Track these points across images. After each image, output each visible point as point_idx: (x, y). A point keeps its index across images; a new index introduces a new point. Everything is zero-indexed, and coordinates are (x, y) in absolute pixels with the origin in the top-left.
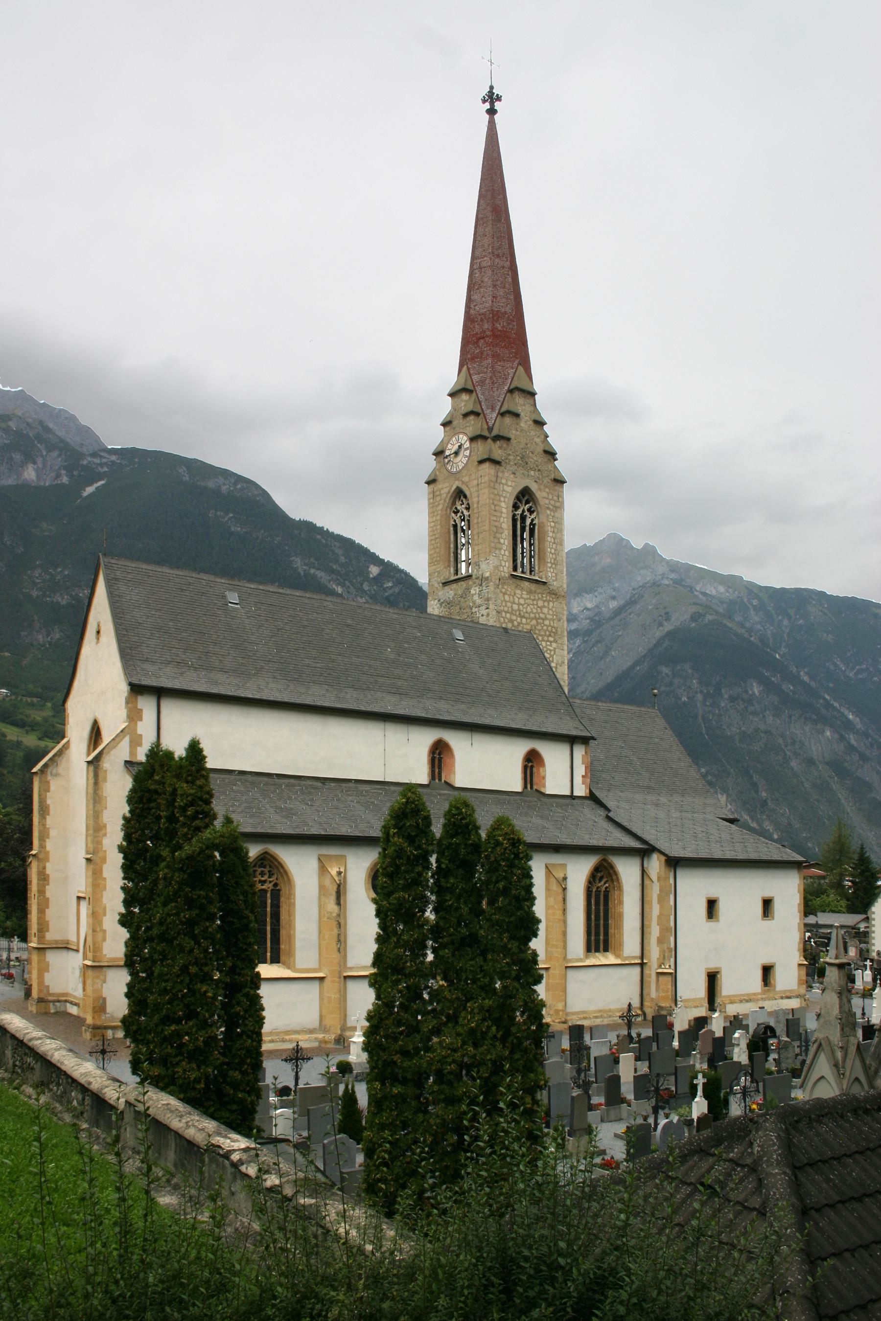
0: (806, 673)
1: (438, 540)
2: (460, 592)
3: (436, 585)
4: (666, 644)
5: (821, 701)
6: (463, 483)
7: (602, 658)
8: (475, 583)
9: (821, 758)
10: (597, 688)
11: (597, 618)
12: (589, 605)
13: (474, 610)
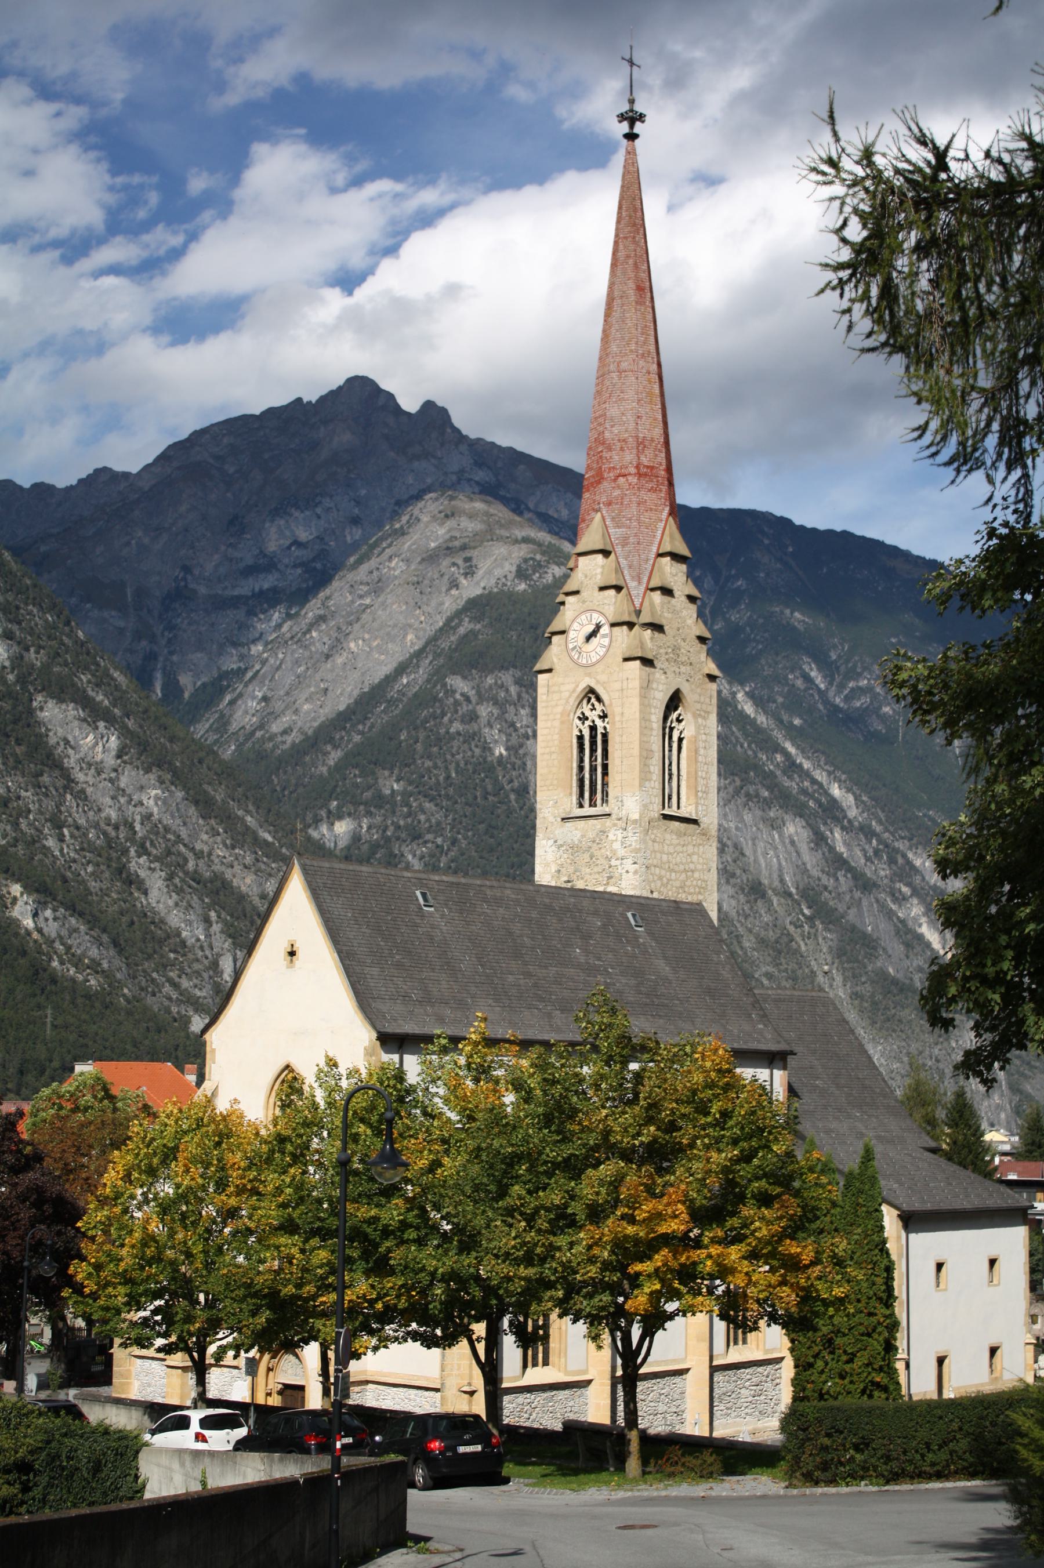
0: (750, 695)
1: (554, 756)
2: (591, 835)
3: (551, 819)
4: (466, 626)
5: (779, 758)
6: (598, 682)
7: (328, 657)
8: (615, 825)
9: (776, 883)
10: (316, 724)
11: (319, 566)
12: (303, 536)
13: (613, 862)
